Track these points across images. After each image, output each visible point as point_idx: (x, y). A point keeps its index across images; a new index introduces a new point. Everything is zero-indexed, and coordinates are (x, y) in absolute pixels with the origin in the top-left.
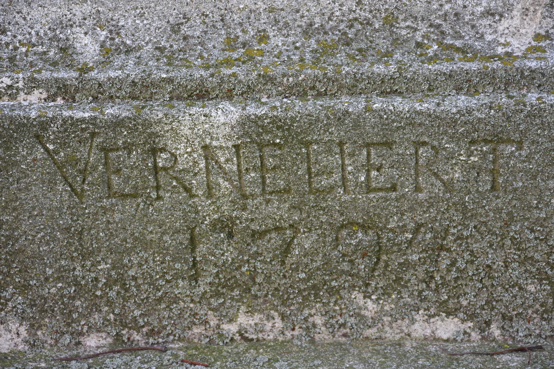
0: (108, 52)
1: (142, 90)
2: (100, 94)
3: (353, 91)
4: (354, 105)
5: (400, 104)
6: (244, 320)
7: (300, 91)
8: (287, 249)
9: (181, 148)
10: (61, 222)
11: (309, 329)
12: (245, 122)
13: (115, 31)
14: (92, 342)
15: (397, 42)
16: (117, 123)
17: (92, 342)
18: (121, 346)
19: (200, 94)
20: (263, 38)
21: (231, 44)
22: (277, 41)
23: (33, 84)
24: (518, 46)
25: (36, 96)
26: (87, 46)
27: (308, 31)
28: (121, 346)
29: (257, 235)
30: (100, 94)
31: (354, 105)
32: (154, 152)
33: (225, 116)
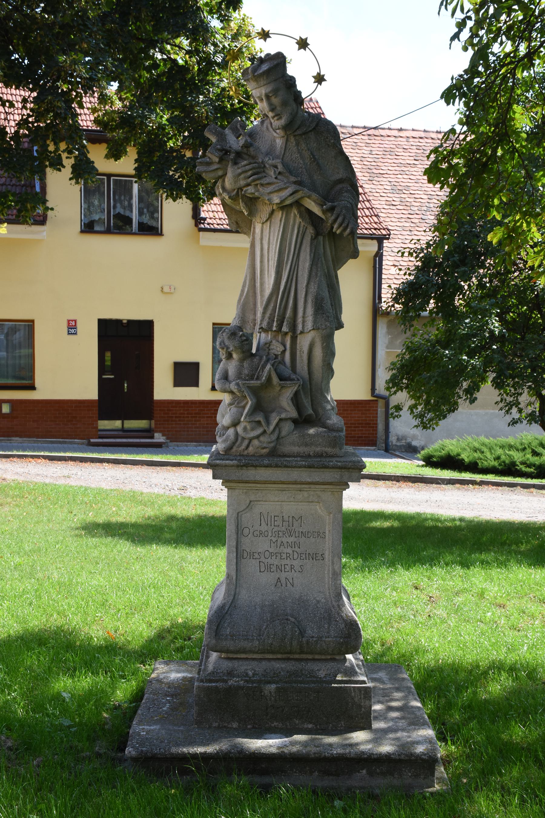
0: (254, 675)
1: (260, 682)
2: (253, 682)
3: (295, 683)
4: (295, 685)
5: (303, 685)
6: (275, 724)
7: (286, 682)
8: (283, 710)
9: (266, 692)
10: (114, 509)
11: (287, 726)
12: (277, 687)
13: (255, 671)
14: (249, 727)
15: (303, 674)
16: (255, 687)
17: (249, 727)
18: (254, 727)
19: (269, 682)
20: (280, 673)
21: (274, 673)
22: (282, 673)
23: (242, 680)
24: (322, 676)
25: (242, 682)
26: (250, 673)
27: (288, 672)
28: (254, 727)
29: (278, 708)
30: (253, 682)
31: (295, 685)
32: (261, 692)
33: (273, 686)
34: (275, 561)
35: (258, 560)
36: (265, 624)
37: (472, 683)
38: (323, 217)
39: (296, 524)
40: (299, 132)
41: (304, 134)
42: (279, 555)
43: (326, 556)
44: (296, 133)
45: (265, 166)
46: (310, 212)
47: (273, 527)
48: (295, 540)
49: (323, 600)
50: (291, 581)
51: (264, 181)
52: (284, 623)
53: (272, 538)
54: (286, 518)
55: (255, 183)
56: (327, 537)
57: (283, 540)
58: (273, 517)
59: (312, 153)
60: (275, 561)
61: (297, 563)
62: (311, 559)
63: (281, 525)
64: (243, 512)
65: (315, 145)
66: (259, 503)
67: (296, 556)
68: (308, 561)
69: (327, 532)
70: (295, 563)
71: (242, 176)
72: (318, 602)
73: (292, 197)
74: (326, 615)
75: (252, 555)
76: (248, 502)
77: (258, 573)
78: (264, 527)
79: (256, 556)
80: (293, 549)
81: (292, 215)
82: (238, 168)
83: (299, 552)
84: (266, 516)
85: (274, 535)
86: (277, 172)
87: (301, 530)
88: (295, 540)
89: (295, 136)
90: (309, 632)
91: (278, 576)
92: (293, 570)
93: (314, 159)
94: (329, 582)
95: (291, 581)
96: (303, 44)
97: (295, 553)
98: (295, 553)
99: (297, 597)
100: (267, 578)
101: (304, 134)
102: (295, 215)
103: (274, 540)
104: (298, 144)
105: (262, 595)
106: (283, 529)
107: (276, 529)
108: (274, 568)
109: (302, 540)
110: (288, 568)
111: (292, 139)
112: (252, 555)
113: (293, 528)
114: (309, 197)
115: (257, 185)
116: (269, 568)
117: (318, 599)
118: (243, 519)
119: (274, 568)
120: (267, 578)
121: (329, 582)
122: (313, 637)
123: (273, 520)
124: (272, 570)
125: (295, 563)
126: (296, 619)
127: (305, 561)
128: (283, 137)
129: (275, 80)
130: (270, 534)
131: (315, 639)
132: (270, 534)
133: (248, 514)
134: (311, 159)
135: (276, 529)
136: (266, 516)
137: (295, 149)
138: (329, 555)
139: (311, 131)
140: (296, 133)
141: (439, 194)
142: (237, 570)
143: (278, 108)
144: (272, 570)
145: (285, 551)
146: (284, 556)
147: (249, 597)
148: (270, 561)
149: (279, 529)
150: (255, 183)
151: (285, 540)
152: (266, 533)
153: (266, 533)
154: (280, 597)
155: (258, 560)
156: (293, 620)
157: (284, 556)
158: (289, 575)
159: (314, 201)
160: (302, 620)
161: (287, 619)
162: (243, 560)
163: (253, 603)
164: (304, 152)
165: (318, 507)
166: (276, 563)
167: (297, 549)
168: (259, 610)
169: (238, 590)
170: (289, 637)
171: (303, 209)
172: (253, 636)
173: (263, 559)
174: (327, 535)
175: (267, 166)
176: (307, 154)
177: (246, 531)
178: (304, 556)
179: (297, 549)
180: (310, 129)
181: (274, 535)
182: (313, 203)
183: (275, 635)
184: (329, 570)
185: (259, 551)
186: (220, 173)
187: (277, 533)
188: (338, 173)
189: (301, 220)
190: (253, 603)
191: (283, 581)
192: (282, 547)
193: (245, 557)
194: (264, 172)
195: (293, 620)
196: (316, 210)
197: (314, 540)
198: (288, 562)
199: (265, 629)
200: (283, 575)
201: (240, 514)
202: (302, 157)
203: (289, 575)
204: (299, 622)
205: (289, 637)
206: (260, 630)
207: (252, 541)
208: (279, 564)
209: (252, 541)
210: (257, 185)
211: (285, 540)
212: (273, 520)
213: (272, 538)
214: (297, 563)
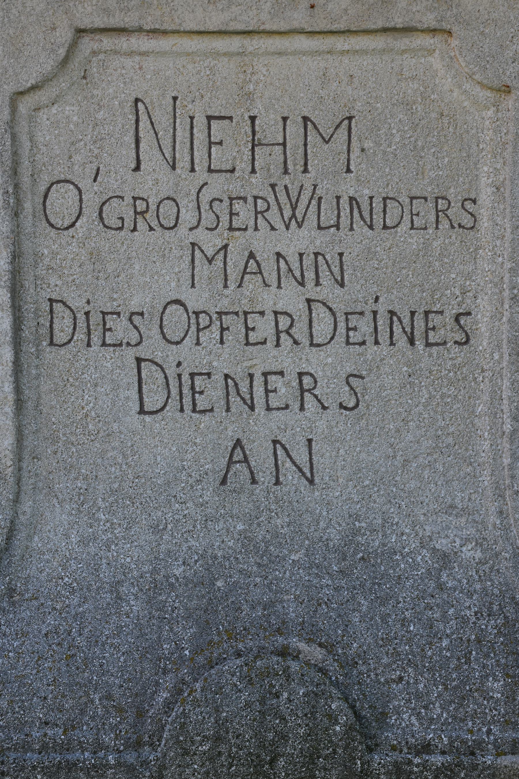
34: (222, 357)
35: (130, 354)
36: (169, 681)
39: (324, 157)
42: (236, 325)
43: (482, 323)
47: (201, 175)
48: (321, 241)
49: (469, 553)
50: (302, 458)
52: (268, 672)
53: (201, 236)
54: (269, 128)
56: (484, 224)
57: (257, 246)
58: (200, 122)
60: (222, 357)
61: (328, 364)
62: (402, 341)
63: (243, 166)
64: (42, 97)
66: (123, 43)
67: (323, 327)
68: (384, 348)
69: (486, 196)
70: (315, 361)
72: (445, 559)
74: (490, 626)
75: (97, 326)
76: (64, 35)
77: (133, 420)
78: (155, 181)
79: (121, 329)
80: (311, 290)
83: (339, 307)
84: (163, 120)
85: (208, 219)
87: (348, 188)
88: (321, 241)
90: (406, 723)
91: (232, 431)
92: (445, 224)
94: (497, 456)
95: (302, 458)
97: (319, 311)
98: (319, 311)
99: (334, 536)
100: (178, 446)
103: (210, 243)
105: (157, 529)
106: (258, 184)
107: (217, 186)
108: (213, 393)
109: (356, 241)
110: (284, 390)
112: (97, 326)
113: (308, 181)
116: (187, 392)
117: (442, 544)
118: (42, 136)
119: (213, 393)
120: (178, 446)
121: (497, 456)
122: (426, 748)
123: (200, 136)
124: (202, 403)
125: (315, 361)
126: (328, 647)
127: (371, 349)
130: (188, 216)
131: (437, 760)
132: (188, 216)
133: (70, 110)
135: (217, 186)
136: (163, 120)
138: (497, 315)
142: (19, 404)
144: (202, 403)
145: (268, 300)
146: (264, 328)
147: (84, 542)
148: (191, 356)
149: (235, 187)
151: (263, 243)
152: (168, 210)
153: (168, 208)
154: (246, 538)
155: (130, 354)
156: (317, 654)
157: (264, 328)
158: (292, 426)
160: (363, 656)
161: (284, 653)
162: (50, 354)
163: (106, 574)
165: (436, 62)
166: (221, 366)
167: (327, 290)
168: (136, 606)
169: (26, 506)
170: (292, 748)
172: (99, 746)
173: (153, 347)
174: (484, 214)
177: (63, 202)
178: (365, 326)
179: (327, 290)
181: (208, 219)
183: (218, 739)
184: (496, 397)
185: (134, 305)
187: (222, 209)
190: (106, 574)
191: (261, 455)
192: (252, 283)
193: (60, 337)
195: (317, 654)
197: (415, 240)
198: (284, 358)
199: (169, 706)
200: (260, 430)
201: (23, 108)
203: (292, 426)
204: (348, 664)
205: (292, 748)
206: (141, 714)
207: (95, 256)
208: (239, 372)
209: (95, 256)
211: (263, 243)
212: (200, 136)
213: (201, 236)
214: (328, 364)
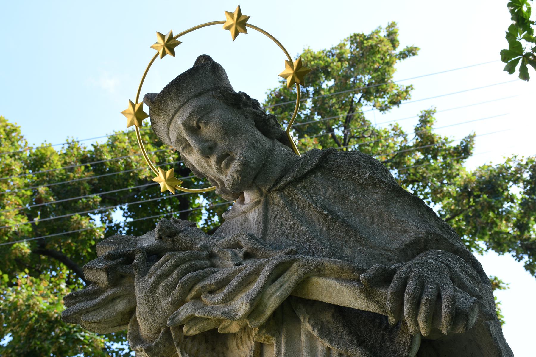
37: (359, 61)
38: (373, 308)
40: (285, 180)
41: (299, 179)
44: (281, 184)
45: (212, 256)
46: (342, 312)
51: (212, 280)
55: (193, 293)
59: (325, 208)
65: (329, 192)
71: (161, 288)
73: (276, 285)
81: (303, 338)
82: (150, 276)
86: (241, 254)
89: (281, 190)
93: (332, 217)
96: (241, 24)
101: (299, 179)
102: (310, 337)
104: (290, 202)
111: (277, 198)
114: (320, 271)
115: (197, 297)
128: (258, 203)
129: (198, 95)
134: (326, 218)
137: (286, 213)
139: (312, 171)
140: (281, 184)
141: (50, 316)
143: (222, 144)
150: (193, 293)
159: (339, 279)
164: (307, 211)
171: (327, 317)
175: (215, 250)
176: (314, 213)
180: (310, 167)
182: (335, 284)
186: (121, 306)
188: (405, 231)
189: (326, 344)
194: (213, 266)
196: (349, 297)
202: (303, 219)
210: (197, 297)
